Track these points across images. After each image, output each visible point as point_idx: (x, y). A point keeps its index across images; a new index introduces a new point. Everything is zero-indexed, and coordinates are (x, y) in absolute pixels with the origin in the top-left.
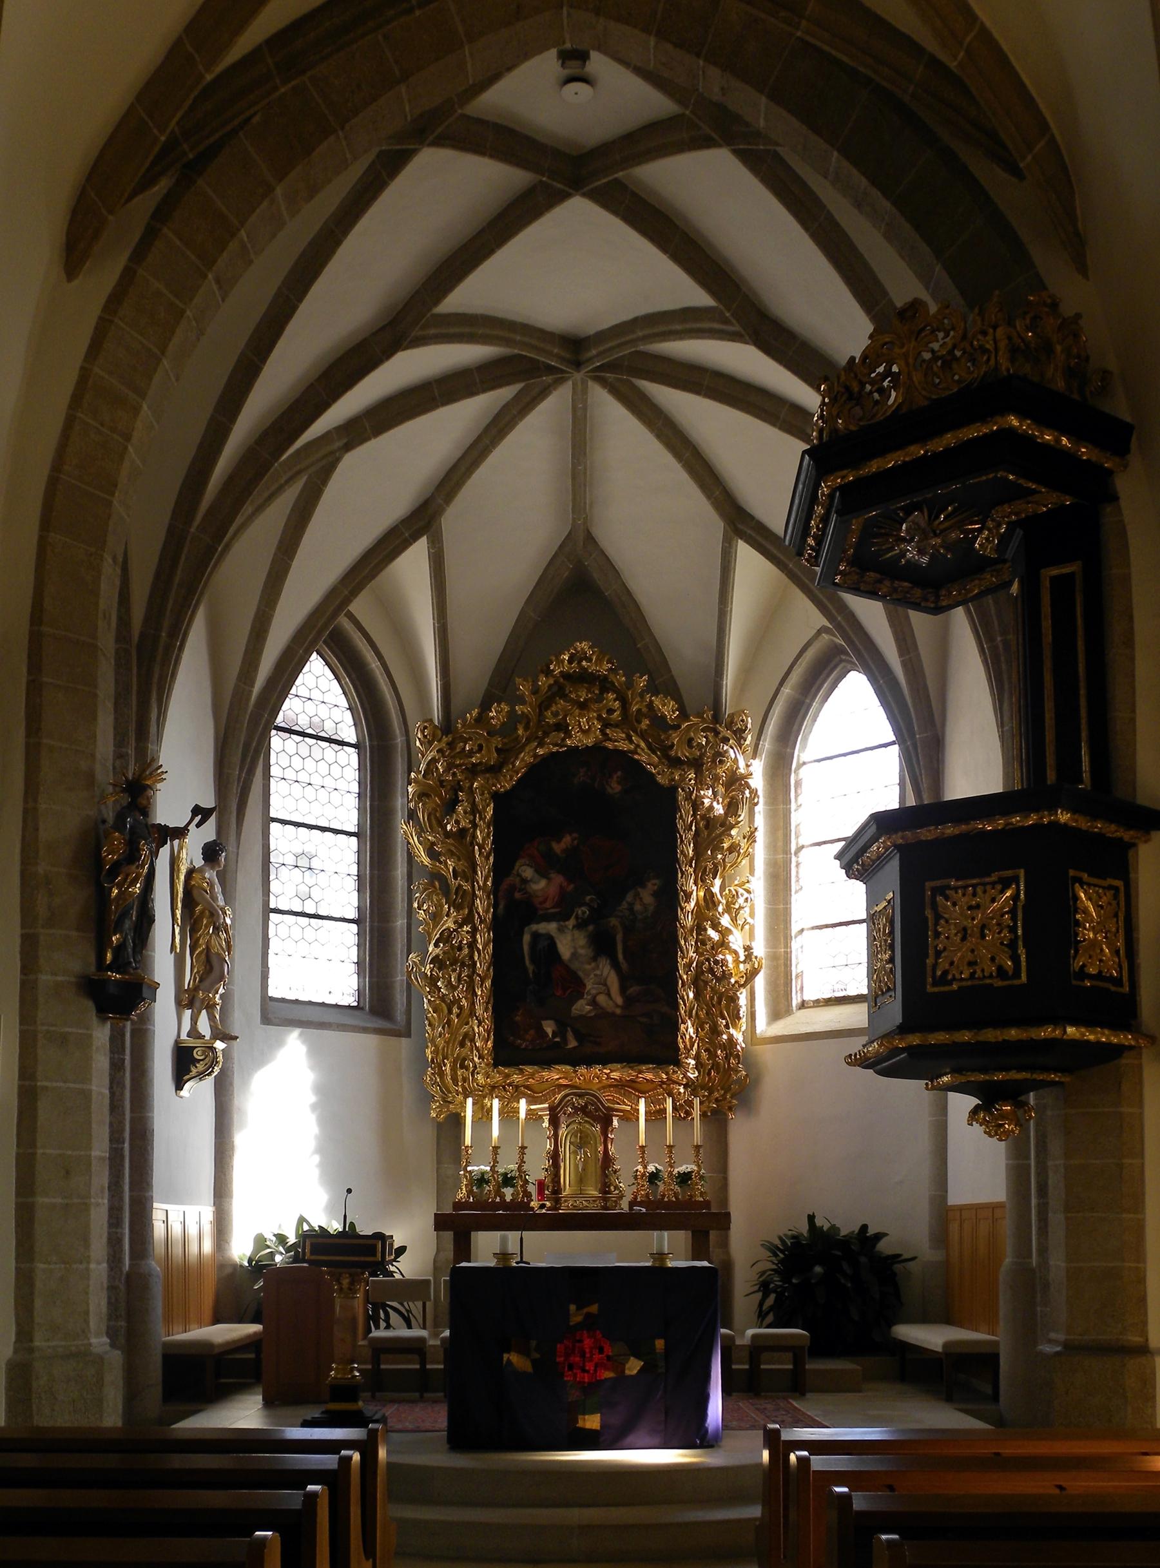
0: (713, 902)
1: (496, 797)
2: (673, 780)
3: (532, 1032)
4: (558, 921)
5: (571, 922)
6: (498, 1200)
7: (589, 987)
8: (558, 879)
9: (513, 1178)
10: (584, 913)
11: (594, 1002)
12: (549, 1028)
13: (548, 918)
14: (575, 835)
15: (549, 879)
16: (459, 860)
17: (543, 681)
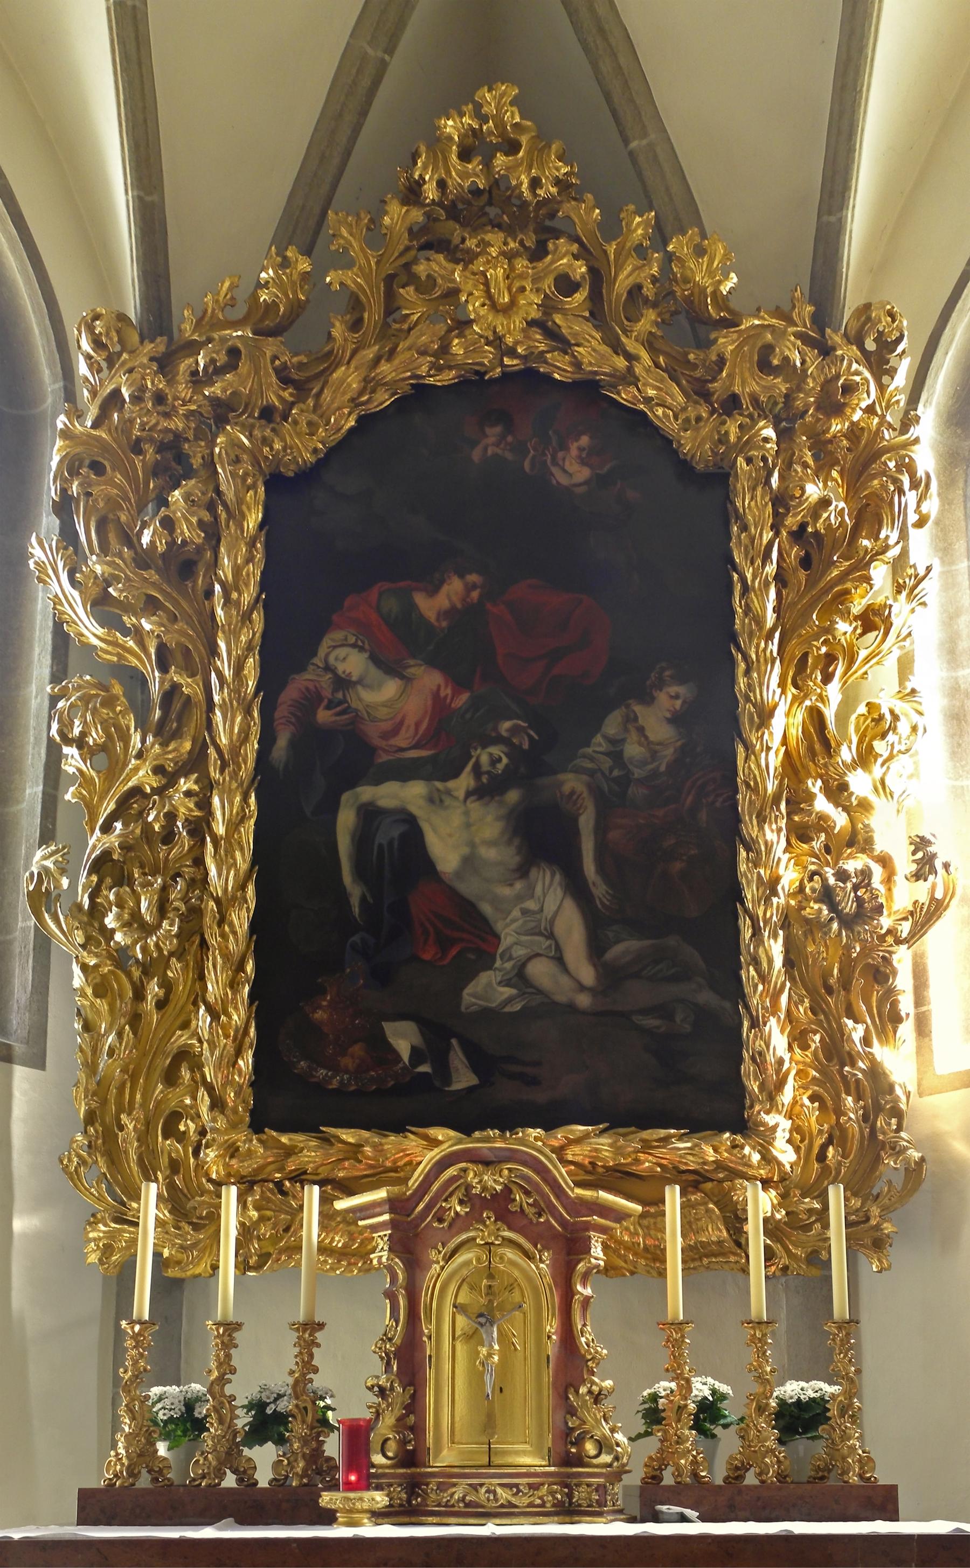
0: (826, 743)
1: (277, 484)
2: (723, 439)
3: (358, 1049)
4: (428, 778)
5: (464, 782)
6: (230, 1481)
7: (507, 939)
8: (430, 680)
9: (281, 1419)
10: (495, 761)
11: (520, 978)
12: (403, 1039)
13: (404, 772)
14: (473, 578)
15: (407, 680)
16: (174, 619)
17: (396, 216)
